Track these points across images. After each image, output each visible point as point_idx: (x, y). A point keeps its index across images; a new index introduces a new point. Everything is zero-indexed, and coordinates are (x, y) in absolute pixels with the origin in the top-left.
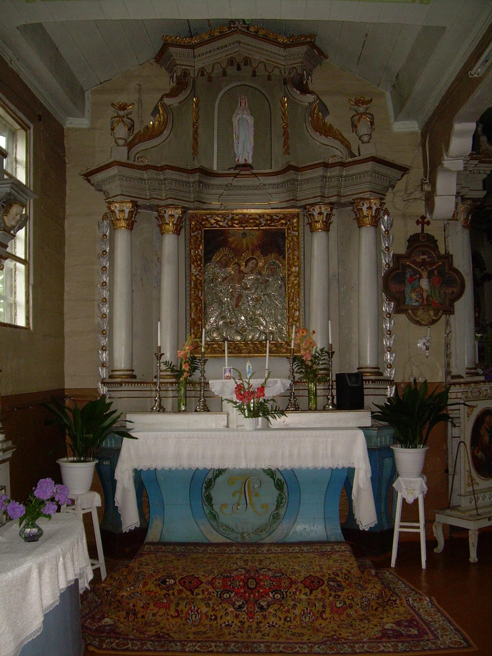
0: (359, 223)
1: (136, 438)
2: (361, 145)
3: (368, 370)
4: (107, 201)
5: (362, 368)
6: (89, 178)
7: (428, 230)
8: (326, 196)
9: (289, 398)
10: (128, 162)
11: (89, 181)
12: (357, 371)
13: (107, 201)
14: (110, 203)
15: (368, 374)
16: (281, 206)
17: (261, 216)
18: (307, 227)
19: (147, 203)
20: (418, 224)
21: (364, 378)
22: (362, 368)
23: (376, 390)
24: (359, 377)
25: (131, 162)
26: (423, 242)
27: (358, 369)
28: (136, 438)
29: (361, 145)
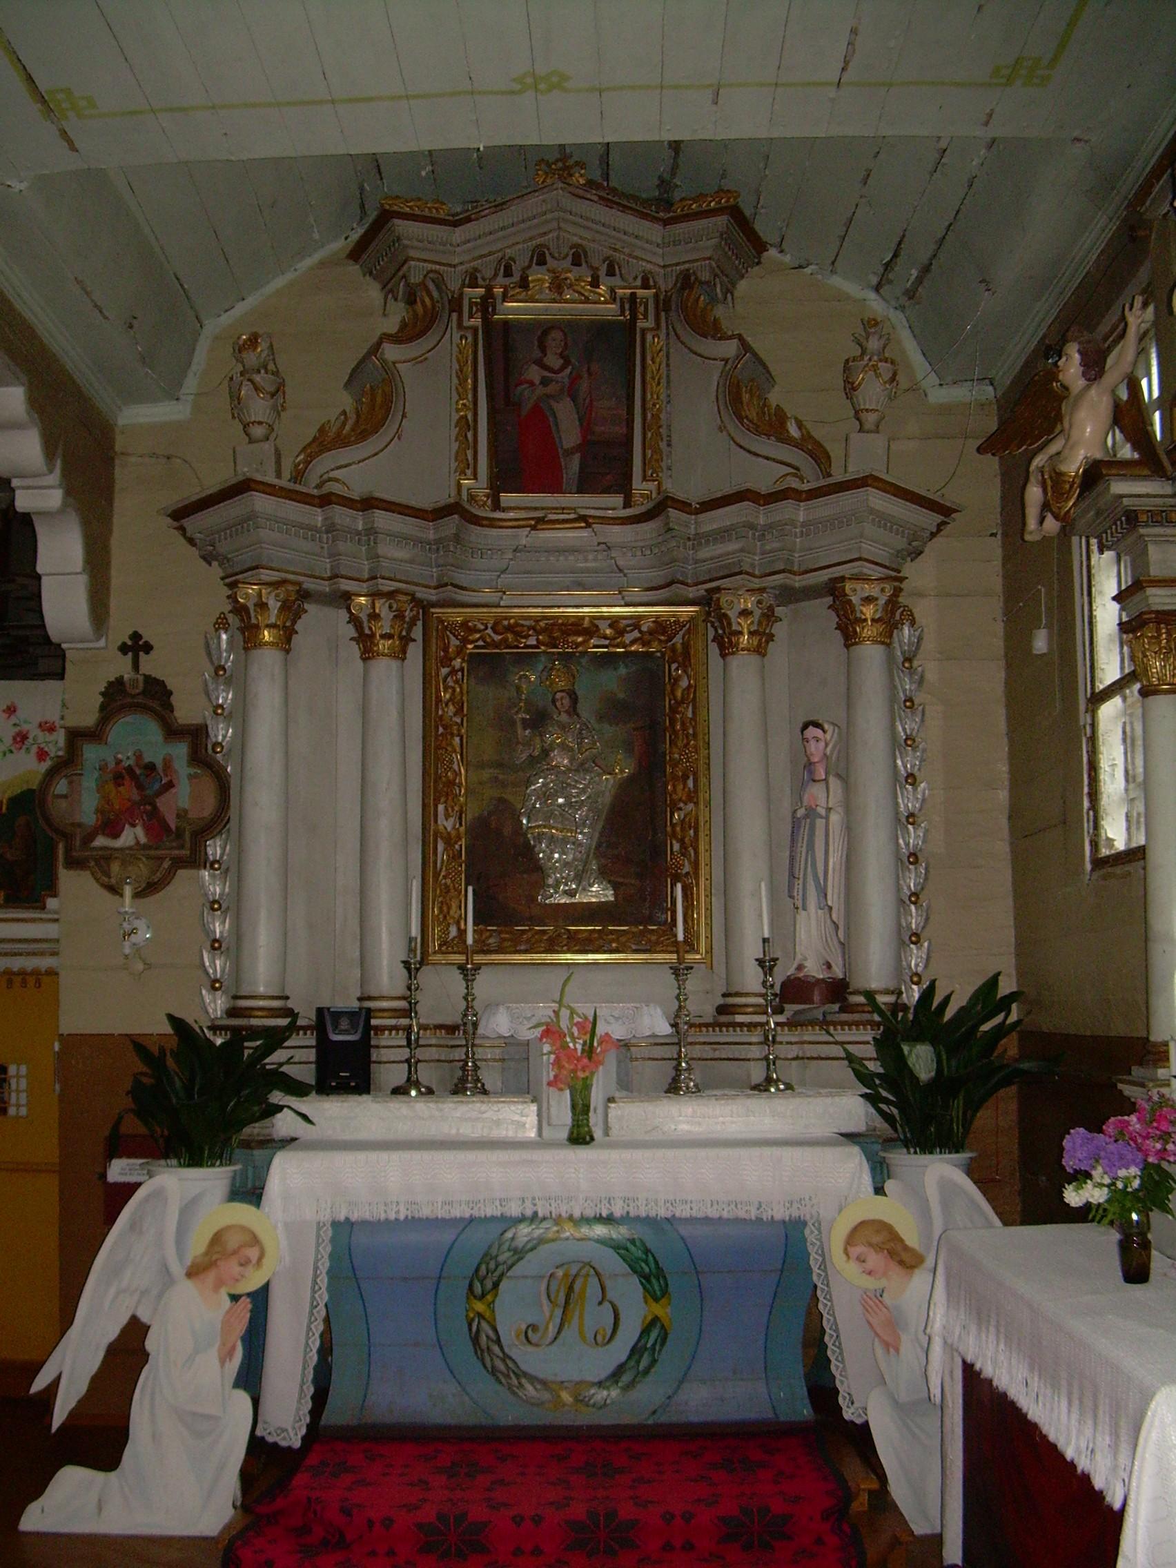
0: (722, 647)
1: (310, 1122)
2: (855, 437)
3: (261, 1003)
4: (227, 581)
5: (370, 998)
6: (186, 522)
7: (150, 665)
8: (796, 568)
9: (675, 1063)
10: (276, 481)
11: (182, 529)
12: (356, 1005)
13: (227, 581)
14: (233, 585)
15: (260, 1013)
16: (645, 599)
17: (636, 621)
18: (714, 649)
19: (326, 587)
20: (125, 654)
21: (374, 1022)
22: (370, 998)
23: (737, 1056)
24: (362, 1018)
25: (284, 483)
26: (133, 696)
27: (360, 999)
28: (310, 1122)
29: (855, 437)
